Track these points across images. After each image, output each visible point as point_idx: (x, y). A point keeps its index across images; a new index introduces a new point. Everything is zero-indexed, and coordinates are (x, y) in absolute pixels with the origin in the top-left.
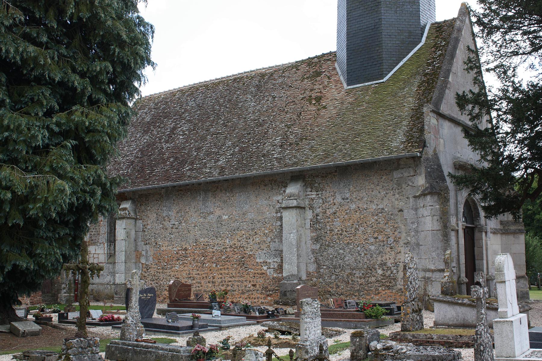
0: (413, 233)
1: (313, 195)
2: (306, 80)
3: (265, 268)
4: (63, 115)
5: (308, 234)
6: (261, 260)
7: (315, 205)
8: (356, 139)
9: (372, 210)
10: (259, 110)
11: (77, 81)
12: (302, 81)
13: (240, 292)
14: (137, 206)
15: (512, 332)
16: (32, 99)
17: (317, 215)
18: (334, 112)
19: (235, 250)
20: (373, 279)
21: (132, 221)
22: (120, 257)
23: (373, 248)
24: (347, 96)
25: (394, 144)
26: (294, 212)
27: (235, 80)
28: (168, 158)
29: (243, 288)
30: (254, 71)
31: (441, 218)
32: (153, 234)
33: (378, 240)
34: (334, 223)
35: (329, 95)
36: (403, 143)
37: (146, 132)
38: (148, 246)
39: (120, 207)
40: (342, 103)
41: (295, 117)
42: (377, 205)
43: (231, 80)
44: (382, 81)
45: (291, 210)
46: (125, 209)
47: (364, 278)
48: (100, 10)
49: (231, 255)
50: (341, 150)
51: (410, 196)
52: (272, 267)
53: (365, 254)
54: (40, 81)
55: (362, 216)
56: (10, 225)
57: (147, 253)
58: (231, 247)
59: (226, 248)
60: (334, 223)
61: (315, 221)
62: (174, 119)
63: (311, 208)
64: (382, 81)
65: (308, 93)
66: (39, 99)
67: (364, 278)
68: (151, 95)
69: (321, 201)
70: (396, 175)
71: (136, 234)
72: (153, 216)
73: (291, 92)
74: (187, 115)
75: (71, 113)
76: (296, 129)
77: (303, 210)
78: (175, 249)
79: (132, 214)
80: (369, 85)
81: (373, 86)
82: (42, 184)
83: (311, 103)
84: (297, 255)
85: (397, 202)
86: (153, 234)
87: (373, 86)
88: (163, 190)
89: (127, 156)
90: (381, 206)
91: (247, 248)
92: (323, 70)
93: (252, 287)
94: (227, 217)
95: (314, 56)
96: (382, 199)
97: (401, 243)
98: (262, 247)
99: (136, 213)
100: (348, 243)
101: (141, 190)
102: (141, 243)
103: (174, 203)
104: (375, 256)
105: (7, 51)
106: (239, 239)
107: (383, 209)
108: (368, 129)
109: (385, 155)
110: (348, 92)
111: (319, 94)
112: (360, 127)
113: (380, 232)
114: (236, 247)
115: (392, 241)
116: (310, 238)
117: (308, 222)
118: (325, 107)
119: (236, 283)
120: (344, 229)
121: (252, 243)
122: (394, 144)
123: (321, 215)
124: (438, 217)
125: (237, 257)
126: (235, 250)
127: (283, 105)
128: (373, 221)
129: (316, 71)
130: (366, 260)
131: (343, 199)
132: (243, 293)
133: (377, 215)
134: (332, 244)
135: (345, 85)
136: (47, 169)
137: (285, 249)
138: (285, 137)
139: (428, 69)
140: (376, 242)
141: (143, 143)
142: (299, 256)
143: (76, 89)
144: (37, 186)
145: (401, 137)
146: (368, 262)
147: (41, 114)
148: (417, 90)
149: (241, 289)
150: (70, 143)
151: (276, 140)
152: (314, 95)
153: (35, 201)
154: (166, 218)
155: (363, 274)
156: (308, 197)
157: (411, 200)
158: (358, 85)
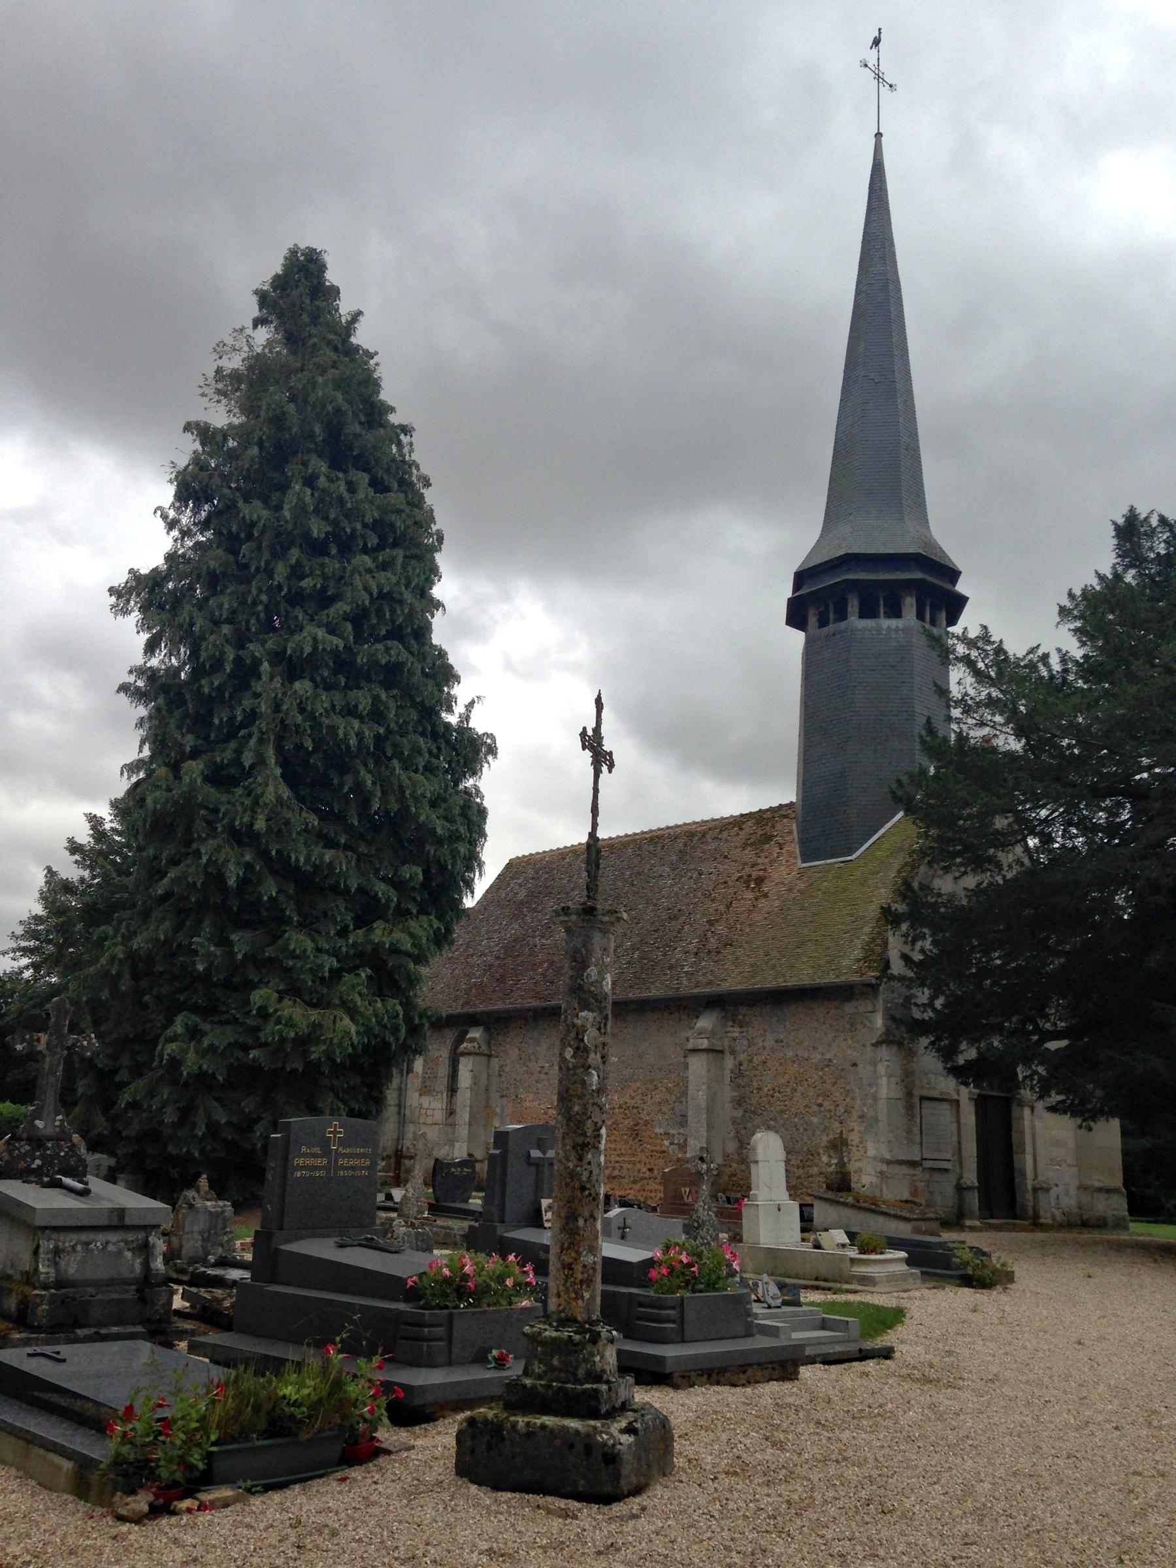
0: (870, 1101)
1: (735, 1032)
2: (749, 848)
3: (666, 1143)
4: (360, 932)
5: (727, 1094)
6: (662, 1131)
7: (737, 1049)
8: (798, 950)
9: (816, 1061)
10: (676, 893)
11: (381, 889)
12: (744, 849)
13: (632, 1179)
14: (491, 1035)
15: (757, 1216)
16: (325, 914)
17: (741, 1064)
18: (777, 903)
19: (627, 1112)
20: (815, 1170)
21: (484, 1059)
22: (464, 1116)
23: (815, 1120)
24: (799, 879)
25: (846, 962)
26: (703, 1058)
27: (652, 839)
28: (541, 963)
29: (636, 1173)
30: (680, 826)
31: (903, 1081)
32: (512, 1081)
33: (822, 1109)
34: (763, 1078)
35: (775, 875)
36: (858, 961)
37: (515, 917)
38: (504, 1099)
39: (468, 1036)
40: (790, 890)
41: (722, 908)
42: (823, 1054)
43: (646, 839)
44: (849, 858)
45: (700, 1053)
46: (473, 1040)
47: (803, 1168)
48: (411, 802)
49: (620, 1119)
50: (773, 967)
51: (868, 1043)
52: (676, 1142)
53: (805, 1130)
54: (334, 889)
55: (802, 1070)
56: (288, 1070)
57: (502, 1111)
58: (620, 1107)
59: (614, 1108)
60: (763, 1078)
61: (738, 1073)
62: (558, 899)
63: (733, 1052)
64: (849, 858)
65: (747, 870)
66: (333, 915)
67: (803, 1168)
68: (531, 855)
69: (746, 1042)
70: (849, 1008)
71: (488, 1080)
72: (514, 1053)
73: (726, 867)
74: (577, 893)
75: (371, 930)
76: (721, 928)
77: (721, 1055)
78: (542, 1106)
79: (484, 1048)
80: (830, 864)
81: (837, 866)
82: (327, 1022)
83: (748, 887)
84: (708, 1125)
85: (849, 1052)
86: (512, 1081)
87: (837, 866)
88: (531, 1013)
89: (485, 955)
90: (828, 1056)
91: (643, 1110)
92: (775, 833)
93: (648, 1173)
94: (616, 1059)
95: (767, 807)
96: (829, 1045)
97: (855, 1115)
98: (664, 1109)
99: (489, 1046)
100: (782, 1111)
101: (498, 1011)
102: (494, 1095)
103: (543, 1034)
104: (818, 1133)
105: (297, 859)
106: (633, 1095)
107: (830, 1060)
108: (816, 936)
109: (830, 978)
110: (802, 873)
111: (761, 873)
112: (806, 931)
113: (826, 1095)
114: (628, 1108)
115: (842, 1111)
116: (729, 1099)
117: (728, 1076)
118: (766, 896)
119: (626, 1166)
120: (777, 1089)
121: (649, 1103)
122: (846, 962)
123: (745, 1064)
124: (898, 1079)
125: (628, 1123)
126: (627, 1112)
127: (710, 888)
128: (817, 1078)
129: (766, 834)
130: (805, 1139)
131: (776, 1041)
132: (635, 1182)
133: (822, 1069)
134: (760, 1111)
135: (799, 860)
136: (337, 1001)
137: (690, 1114)
138: (704, 939)
139: (918, 843)
140: (820, 1112)
141: (509, 935)
142: (710, 1127)
143: (379, 900)
144: (320, 1026)
145: (857, 953)
146: (809, 1142)
147: (332, 933)
148: (895, 877)
149: (632, 1175)
150: (364, 973)
151: (691, 943)
152: (755, 875)
153: (318, 1041)
154: (532, 1057)
155: (801, 1161)
156: (729, 1034)
157: (869, 1049)
158: (817, 863)
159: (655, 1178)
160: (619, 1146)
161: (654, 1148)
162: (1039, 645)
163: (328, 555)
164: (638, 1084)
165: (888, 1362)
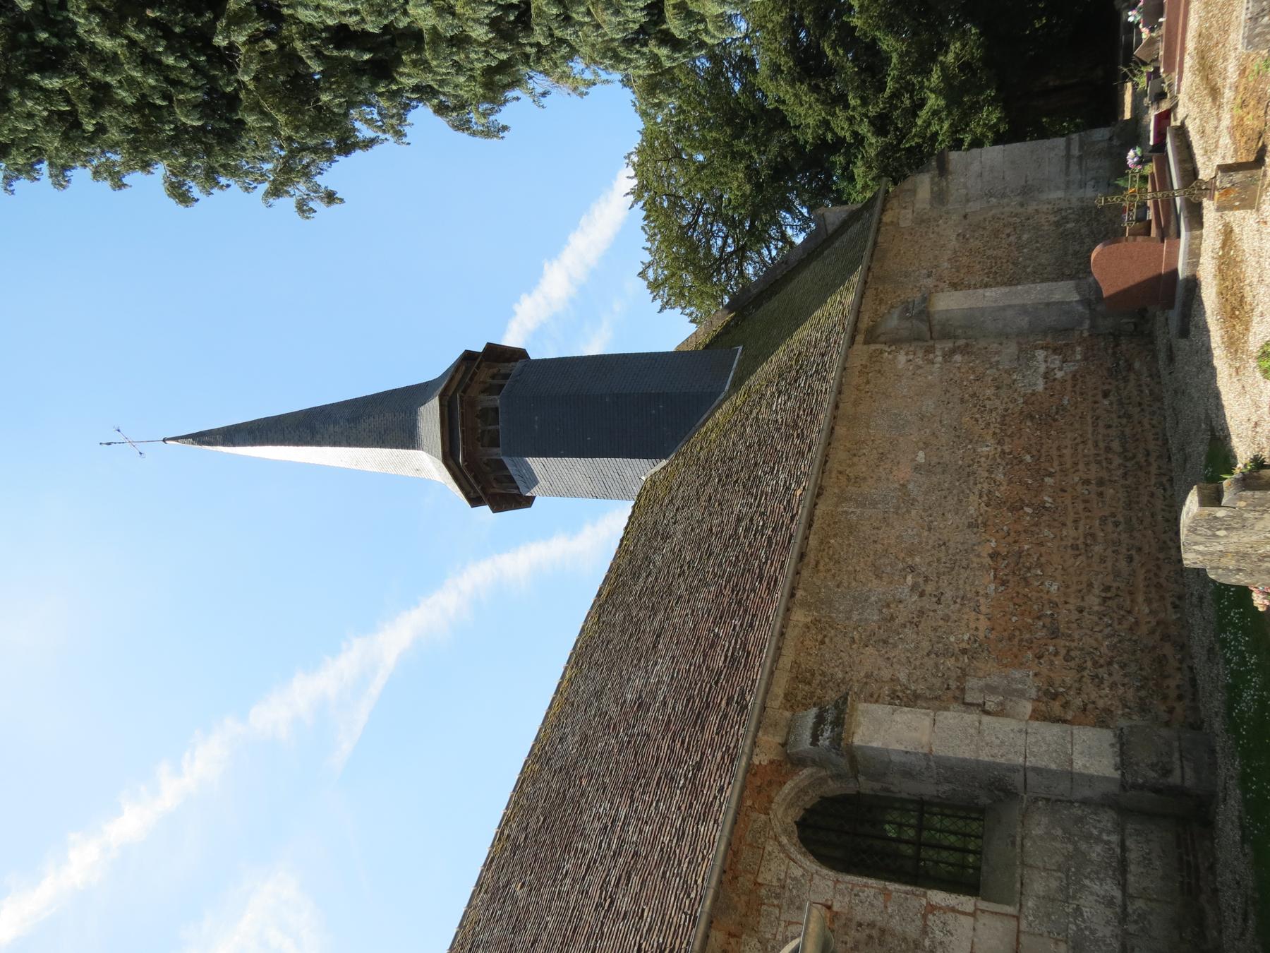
93: (1112, 398)
159: (1118, 388)
160: (1068, 442)
161: (1069, 388)
162: (660, 311)
163: (286, 45)
164: (966, 419)
165: (945, 713)
